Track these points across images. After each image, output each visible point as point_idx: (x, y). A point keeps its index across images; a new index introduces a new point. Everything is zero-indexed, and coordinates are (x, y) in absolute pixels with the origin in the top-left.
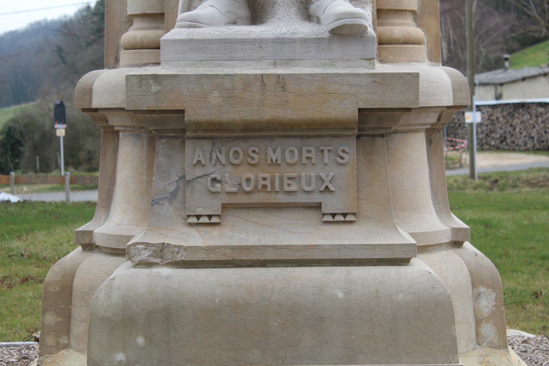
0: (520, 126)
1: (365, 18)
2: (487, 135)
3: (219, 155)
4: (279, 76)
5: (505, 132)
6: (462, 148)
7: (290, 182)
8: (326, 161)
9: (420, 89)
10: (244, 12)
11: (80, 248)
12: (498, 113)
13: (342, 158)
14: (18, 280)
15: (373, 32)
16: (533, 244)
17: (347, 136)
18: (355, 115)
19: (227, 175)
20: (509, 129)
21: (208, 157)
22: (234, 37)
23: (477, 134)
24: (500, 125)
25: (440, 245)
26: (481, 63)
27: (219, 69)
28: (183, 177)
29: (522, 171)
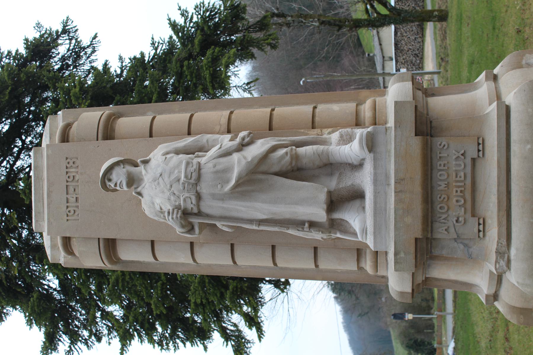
0: (408, 46)
1: (363, 133)
2: (413, 65)
3: (442, 218)
4: (396, 182)
5: (412, 54)
6: (421, 79)
7: (458, 176)
8: (446, 155)
9: (403, 100)
10: (357, 203)
11: (496, 303)
12: (401, 59)
13: (444, 146)
14: (506, 344)
15: (370, 128)
16: (485, 35)
17: (431, 143)
18: (419, 138)
19: (454, 214)
20: (410, 52)
21: (443, 225)
22: (373, 208)
23: (413, 71)
24: (407, 58)
25: (496, 88)
26: (371, 70)
27: (391, 217)
28: (455, 240)
29: (436, 44)
